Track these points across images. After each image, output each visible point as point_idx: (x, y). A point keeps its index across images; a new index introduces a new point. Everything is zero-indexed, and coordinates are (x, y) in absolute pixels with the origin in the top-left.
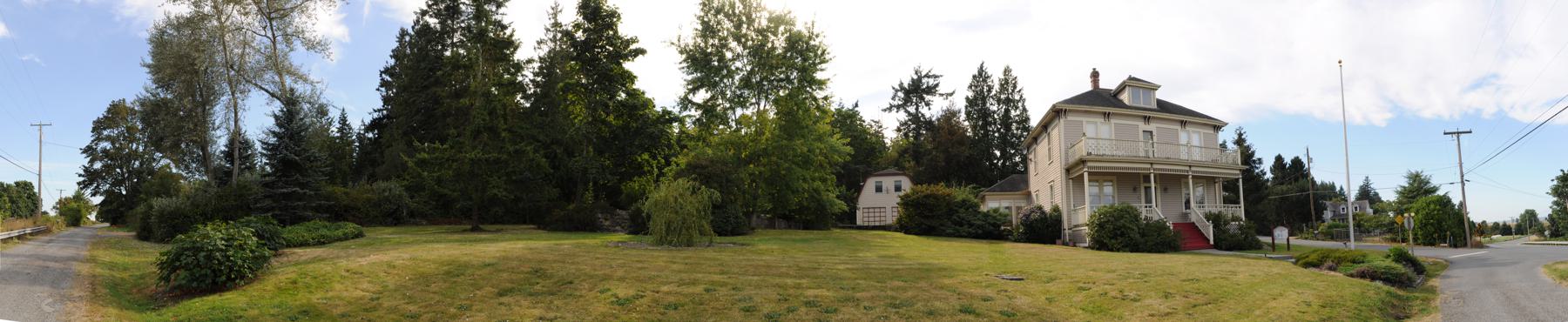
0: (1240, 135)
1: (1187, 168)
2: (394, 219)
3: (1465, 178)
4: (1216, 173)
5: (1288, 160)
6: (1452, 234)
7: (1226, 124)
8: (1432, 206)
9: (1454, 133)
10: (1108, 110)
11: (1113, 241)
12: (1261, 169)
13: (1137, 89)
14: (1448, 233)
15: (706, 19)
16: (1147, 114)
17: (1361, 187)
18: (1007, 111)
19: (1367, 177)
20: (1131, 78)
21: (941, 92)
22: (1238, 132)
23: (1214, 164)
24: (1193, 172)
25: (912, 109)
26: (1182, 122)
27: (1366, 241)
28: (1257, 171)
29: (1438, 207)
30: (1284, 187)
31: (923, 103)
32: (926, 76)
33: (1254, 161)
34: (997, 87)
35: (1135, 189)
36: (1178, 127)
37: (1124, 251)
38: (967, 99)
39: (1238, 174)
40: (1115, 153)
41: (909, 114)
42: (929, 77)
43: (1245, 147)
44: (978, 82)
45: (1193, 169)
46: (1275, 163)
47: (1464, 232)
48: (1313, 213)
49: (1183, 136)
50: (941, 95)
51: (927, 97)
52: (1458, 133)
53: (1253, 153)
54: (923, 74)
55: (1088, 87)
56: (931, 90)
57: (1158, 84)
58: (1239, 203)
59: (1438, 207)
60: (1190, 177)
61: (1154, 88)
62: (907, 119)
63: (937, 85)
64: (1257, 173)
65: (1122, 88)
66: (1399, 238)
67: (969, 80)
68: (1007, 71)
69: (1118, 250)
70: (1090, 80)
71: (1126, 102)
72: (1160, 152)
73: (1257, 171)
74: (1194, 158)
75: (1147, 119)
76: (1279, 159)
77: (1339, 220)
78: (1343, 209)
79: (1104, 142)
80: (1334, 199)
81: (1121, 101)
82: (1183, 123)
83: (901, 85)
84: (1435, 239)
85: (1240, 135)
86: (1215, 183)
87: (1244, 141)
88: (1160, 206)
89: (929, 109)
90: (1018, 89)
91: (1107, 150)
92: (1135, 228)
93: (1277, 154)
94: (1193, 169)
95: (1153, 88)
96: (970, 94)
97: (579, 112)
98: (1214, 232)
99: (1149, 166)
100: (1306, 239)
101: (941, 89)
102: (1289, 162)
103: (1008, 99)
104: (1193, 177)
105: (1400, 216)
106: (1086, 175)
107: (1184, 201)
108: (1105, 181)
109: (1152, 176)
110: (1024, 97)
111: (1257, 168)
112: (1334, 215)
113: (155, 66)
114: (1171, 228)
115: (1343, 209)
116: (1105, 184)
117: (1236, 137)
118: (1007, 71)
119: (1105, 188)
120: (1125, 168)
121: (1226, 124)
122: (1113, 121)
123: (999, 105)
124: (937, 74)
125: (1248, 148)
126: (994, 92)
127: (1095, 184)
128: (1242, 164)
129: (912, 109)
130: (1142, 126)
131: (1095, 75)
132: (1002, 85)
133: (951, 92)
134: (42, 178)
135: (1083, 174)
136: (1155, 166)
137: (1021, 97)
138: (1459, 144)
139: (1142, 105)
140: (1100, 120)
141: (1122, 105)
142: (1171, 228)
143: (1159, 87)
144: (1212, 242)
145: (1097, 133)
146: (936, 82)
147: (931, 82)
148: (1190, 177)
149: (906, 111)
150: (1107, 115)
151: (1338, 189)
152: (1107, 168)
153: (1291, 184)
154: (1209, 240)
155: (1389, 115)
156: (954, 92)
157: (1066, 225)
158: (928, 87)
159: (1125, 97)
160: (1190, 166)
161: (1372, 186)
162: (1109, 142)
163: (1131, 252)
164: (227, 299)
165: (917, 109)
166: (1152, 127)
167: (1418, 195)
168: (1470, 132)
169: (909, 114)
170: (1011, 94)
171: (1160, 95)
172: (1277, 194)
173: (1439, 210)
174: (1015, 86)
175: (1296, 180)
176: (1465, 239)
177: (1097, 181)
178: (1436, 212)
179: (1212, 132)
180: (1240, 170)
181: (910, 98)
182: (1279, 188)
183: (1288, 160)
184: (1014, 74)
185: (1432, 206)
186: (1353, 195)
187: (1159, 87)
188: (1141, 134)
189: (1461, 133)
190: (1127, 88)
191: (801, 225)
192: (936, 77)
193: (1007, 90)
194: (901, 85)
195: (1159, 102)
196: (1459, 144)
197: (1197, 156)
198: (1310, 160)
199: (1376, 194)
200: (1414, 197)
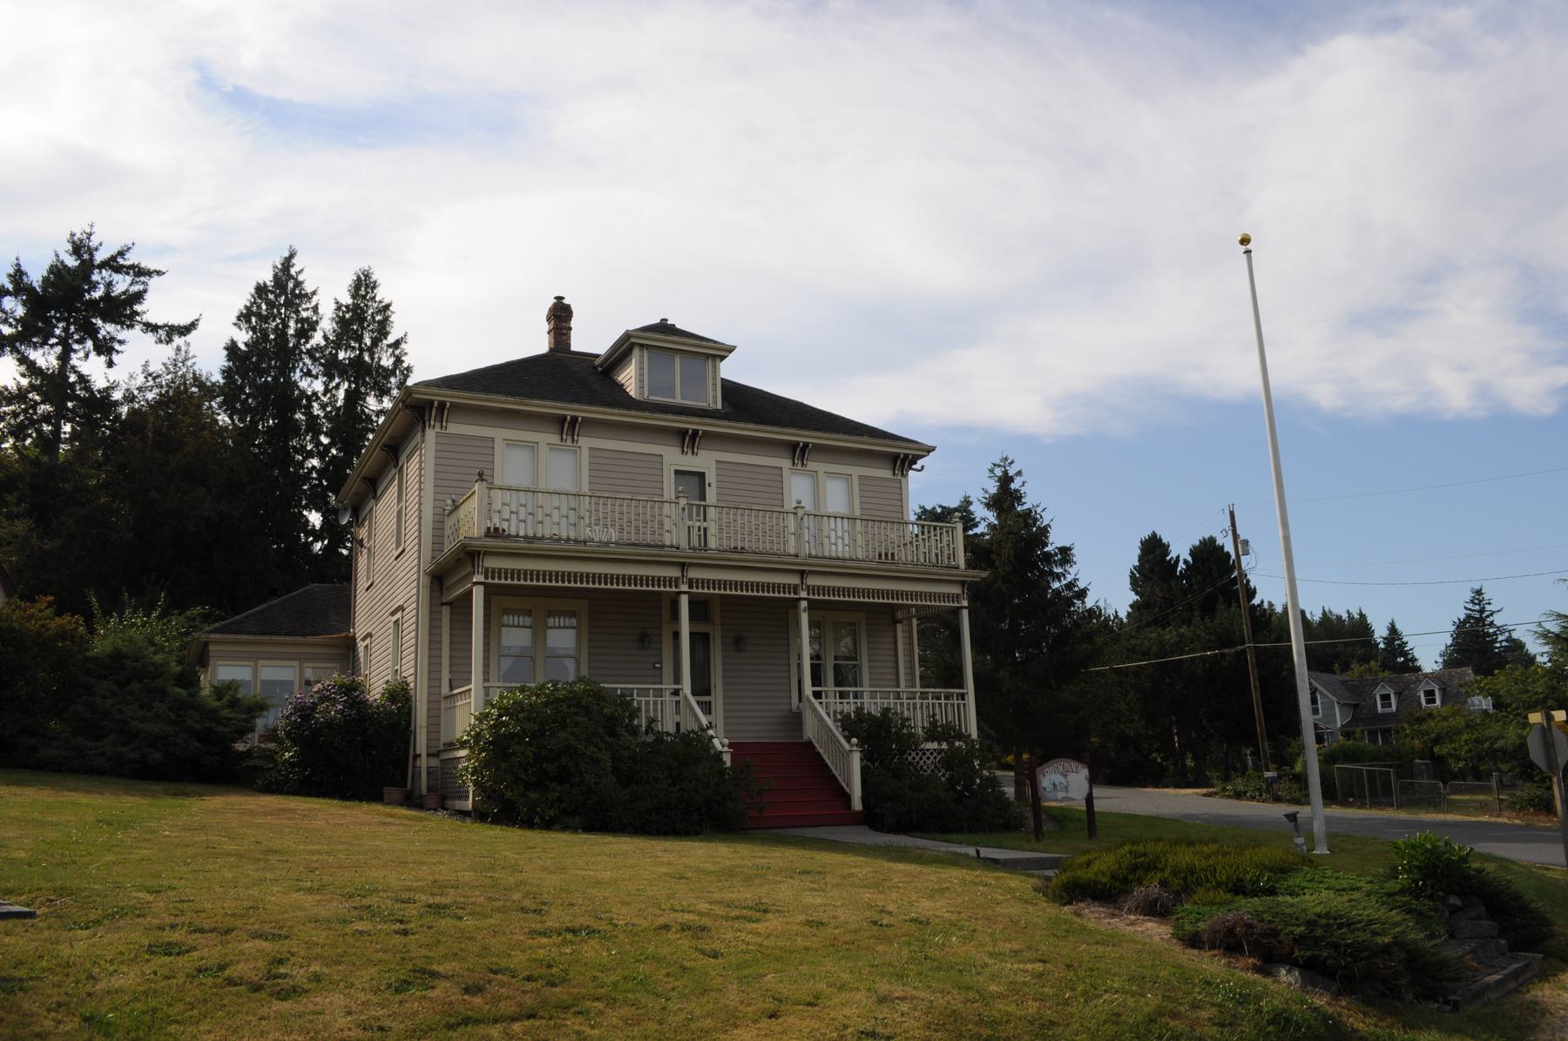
0: (1006, 480)
1: (795, 580)
4: (898, 594)
5: (1180, 549)
7: (930, 450)
11: (533, 796)
12: (1070, 578)
15: (526, 930)
16: (691, 424)
17: (1461, 625)
18: (354, 397)
19: (1479, 592)
20: (664, 328)
21: (151, 318)
22: (998, 472)
23: (885, 568)
24: (809, 589)
25: (46, 358)
26: (793, 446)
27: (1452, 807)
28: (1056, 585)
30: (1169, 635)
31: (89, 344)
32: (104, 265)
33: (1048, 557)
34: (327, 325)
36: (785, 463)
37: (564, 829)
38: (232, 349)
39: (957, 598)
40: (586, 533)
41: (31, 368)
42: (118, 269)
43: (1019, 515)
44: (271, 304)
45: (812, 581)
46: (1141, 558)
48: (1258, 712)
49: (798, 487)
50: (151, 328)
51: (107, 329)
53: (1044, 531)
54: (100, 257)
55: (539, 344)
56: (122, 309)
57: (728, 342)
58: (960, 684)
60: (804, 604)
61: (720, 352)
62: (25, 382)
63: (138, 297)
64: (1057, 592)
65: (625, 348)
67: (242, 298)
68: (363, 285)
69: (548, 825)
70: (546, 327)
71: (632, 390)
73: (1056, 585)
74: (796, 543)
75: (689, 440)
76: (1153, 548)
77: (1373, 734)
78: (1386, 698)
79: (555, 500)
80: (1356, 668)
81: (621, 387)
82: (799, 452)
83: (18, 275)
85: (1006, 480)
86: (896, 621)
87: (1017, 497)
88: (717, 698)
89: (110, 364)
90: (391, 339)
91: (557, 523)
92: (605, 756)
93: (1146, 534)
94: (812, 581)
95: (718, 352)
96: (243, 337)
98: (864, 769)
99: (795, 580)
100: (1238, 796)
101: (154, 309)
102: (1186, 555)
103: (357, 363)
104: (700, 608)
106: (478, 595)
108: (551, 614)
109: (684, 601)
110: (407, 361)
111: (1058, 577)
112: (1355, 720)
114: (727, 758)
115: (1386, 698)
116: (551, 621)
117: (993, 488)
118: (363, 285)
121: (930, 450)
122: (586, 442)
123: (331, 378)
124: (146, 264)
125: (1029, 517)
126: (317, 339)
129: (46, 358)
130: (673, 458)
131: (560, 315)
132: (342, 323)
133: (184, 321)
135: (470, 593)
136: (694, 574)
137: (398, 361)
139: (678, 400)
140: (546, 438)
141: (626, 402)
142: (727, 758)
143: (731, 349)
144: (857, 805)
145: (535, 475)
146: (135, 288)
147: (122, 284)
148: (804, 604)
149: (23, 360)
150: (568, 427)
151: (1380, 632)
152: (538, 575)
153: (1189, 622)
154: (847, 798)
156: (192, 326)
158: (107, 297)
159: (629, 377)
160: (802, 574)
161: (1498, 620)
162: (573, 502)
163: (589, 829)
165: (64, 358)
166: (705, 461)
169: (31, 368)
170: (371, 350)
171: (730, 370)
172: (1146, 655)
174: (382, 330)
175: (1208, 608)
177: (528, 613)
179: (888, 474)
180: (963, 583)
181: (47, 321)
182: (1153, 634)
183: (1180, 549)
184: (382, 294)
186: (1429, 653)
187: (731, 349)
188: (669, 489)
190: (636, 352)
192: (139, 272)
193: (359, 339)
194: (18, 275)
195: (733, 392)
197: (839, 543)
198: (1242, 545)
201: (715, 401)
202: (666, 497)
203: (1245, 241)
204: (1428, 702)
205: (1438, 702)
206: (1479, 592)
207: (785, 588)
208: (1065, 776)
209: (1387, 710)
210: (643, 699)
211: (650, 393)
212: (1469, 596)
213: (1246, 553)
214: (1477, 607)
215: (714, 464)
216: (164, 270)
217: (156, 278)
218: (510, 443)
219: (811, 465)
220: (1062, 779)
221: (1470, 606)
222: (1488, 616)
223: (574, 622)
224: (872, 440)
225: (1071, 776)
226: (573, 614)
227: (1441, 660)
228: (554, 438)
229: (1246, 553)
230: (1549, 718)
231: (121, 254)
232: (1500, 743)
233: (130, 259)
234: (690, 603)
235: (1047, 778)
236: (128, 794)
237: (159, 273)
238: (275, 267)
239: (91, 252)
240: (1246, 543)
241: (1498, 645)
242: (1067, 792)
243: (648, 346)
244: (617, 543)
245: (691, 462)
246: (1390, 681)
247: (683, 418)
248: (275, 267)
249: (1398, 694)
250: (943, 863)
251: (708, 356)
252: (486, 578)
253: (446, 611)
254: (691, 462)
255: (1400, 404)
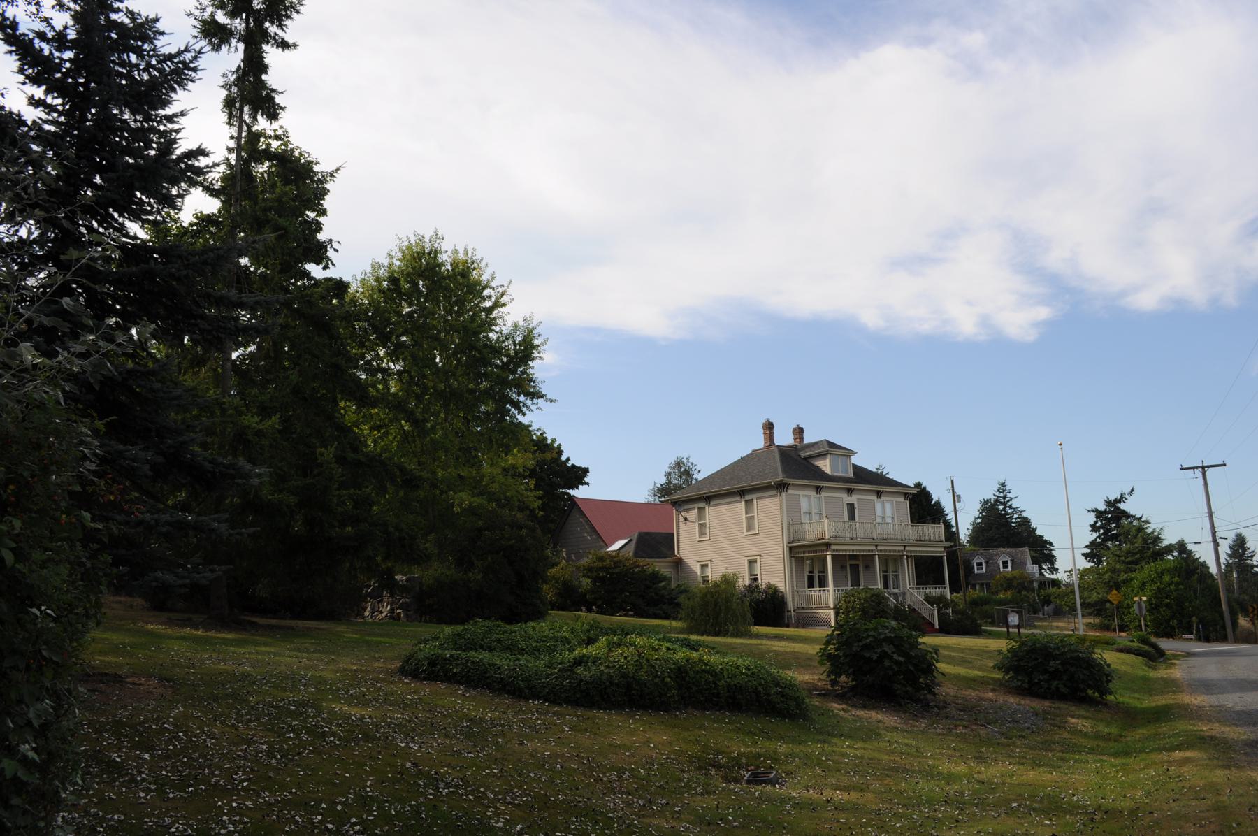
1: (903, 549)
3: (1219, 535)
6: (1201, 621)
8: (1167, 578)
9: (1197, 468)
13: (836, 457)
14: (1194, 618)
19: (1003, 485)
24: (908, 551)
29: (1176, 579)
36: (875, 498)
47: (1222, 617)
52: (1203, 467)
59: (1176, 579)
66: (1116, 624)
71: (828, 471)
74: (879, 532)
78: (979, 564)
82: (879, 494)
84: (1173, 628)
95: (848, 453)
105: (1115, 592)
107: (807, 573)
115: (979, 564)
128: (946, 541)
138: (1206, 484)
154: (933, 625)
155: (1043, 313)
157: (790, 607)
161: (1015, 504)
164: (1057, 627)
166: (853, 499)
167: (1142, 558)
168: (1225, 465)
171: (855, 460)
173: (1177, 584)
176: (1224, 628)
178: (1172, 587)
185: (1167, 578)
186: (965, 522)
189: (1209, 467)
195: (855, 467)
196: (1206, 484)
199: (1025, 522)
200: (1135, 563)
201: (850, 474)
203: (1060, 445)
204: (1004, 567)
205: (1010, 568)
206: (1003, 485)
209: (980, 572)
212: (996, 487)
213: (959, 501)
214: (1002, 495)
218: (803, 495)
221: (997, 494)
222: (1008, 501)
227: (971, 528)
229: (959, 501)
230: (1141, 599)
232: (1089, 600)
240: (959, 496)
241: (1014, 521)
246: (981, 554)
249: (987, 562)
250: (489, 686)
253: (793, 559)
255: (926, 328)
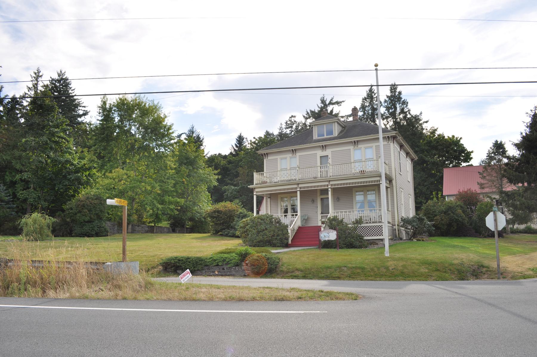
2: (203, 224)
10: (294, 148)
16: (324, 143)
35: (313, 201)
54: (327, 102)
72: (332, 171)
94: (332, 183)
97: (85, 186)
104: (335, 190)
108: (368, 191)
113: (161, 122)
116: (369, 193)
119: (357, 196)
120: (278, 190)
122: (298, 154)
127: (373, 192)
134: (450, 194)
140: (289, 155)
166: (328, 152)
177: (362, 191)
191: (20, 214)
202: (318, 166)
207: (294, 188)
208: (328, 234)
210: (342, 214)
211: (318, 136)
215: (331, 152)
216: (344, 100)
217: (343, 103)
219: (359, 146)
220: (328, 234)
223: (374, 192)
224: (374, 135)
225: (330, 234)
226: (374, 190)
228: (291, 155)
231: (331, 100)
233: (334, 101)
234: (257, 198)
235: (323, 234)
236: (223, 240)
237: (343, 101)
238: (367, 91)
239: (325, 102)
242: (329, 238)
243: (317, 125)
244: (332, 176)
245: (324, 153)
247: (331, 141)
248: (367, 91)
251: (333, 122)
252: (300, 189)
254: (324, 153)
